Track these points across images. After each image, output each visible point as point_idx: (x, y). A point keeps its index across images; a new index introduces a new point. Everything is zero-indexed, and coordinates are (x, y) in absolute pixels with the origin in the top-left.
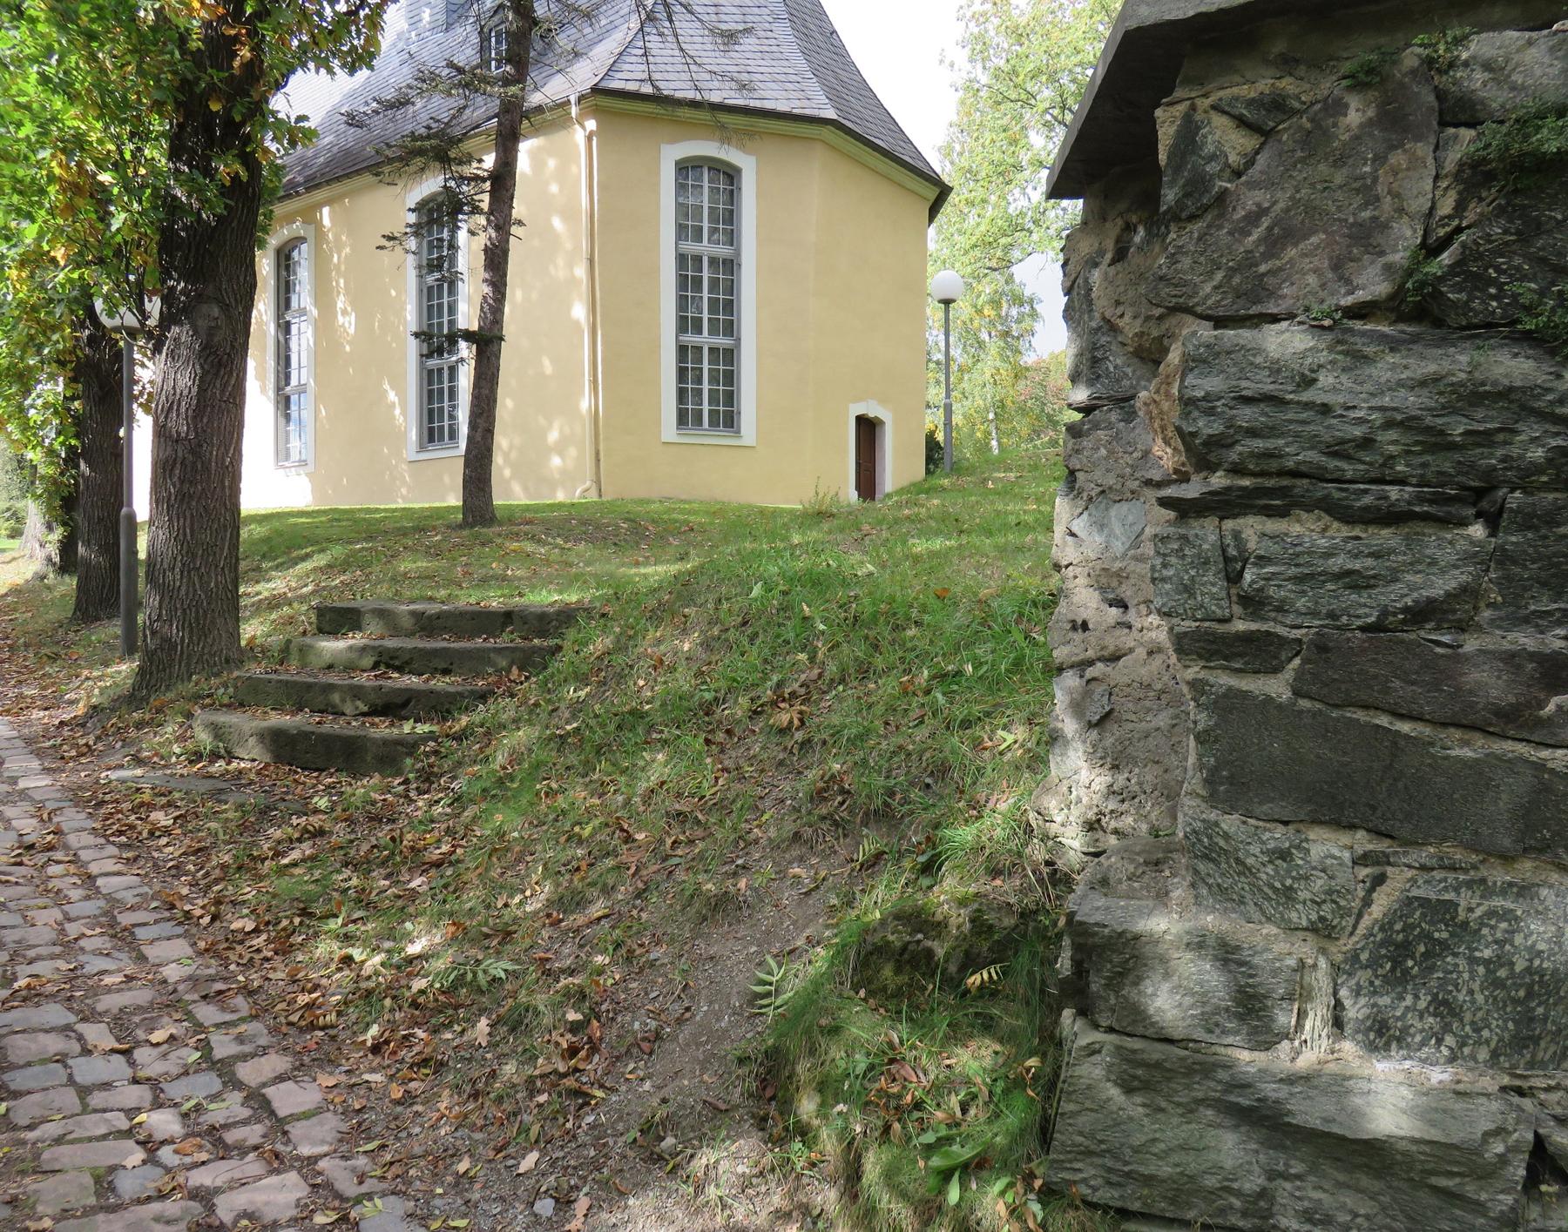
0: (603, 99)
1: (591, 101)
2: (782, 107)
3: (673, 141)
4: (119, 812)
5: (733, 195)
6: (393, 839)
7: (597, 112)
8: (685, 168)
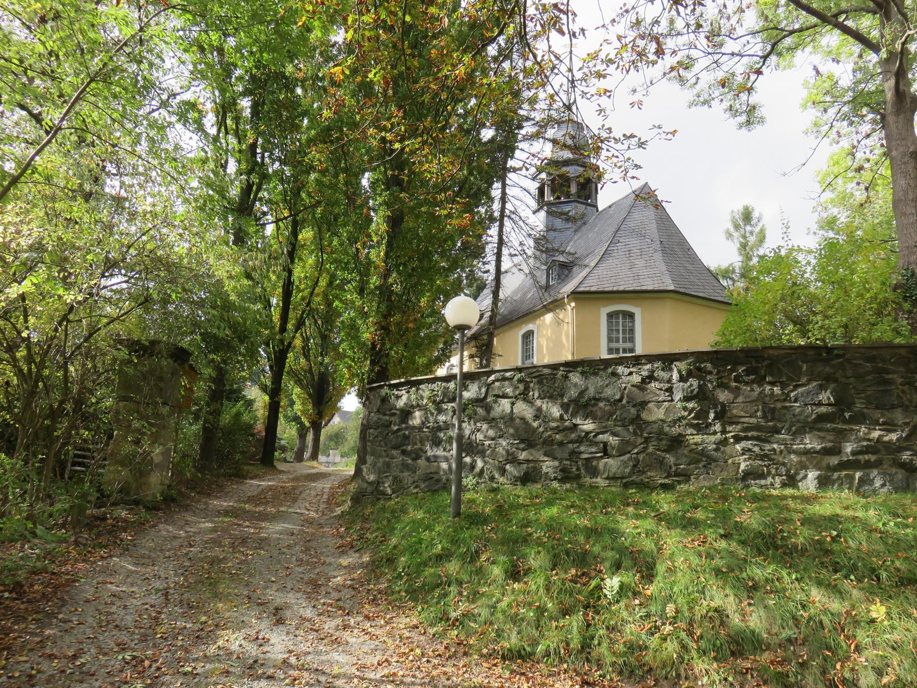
0: (577, 295)
1: (573, 296)
2: (650, 288)
3: (607, 306)
4: (149, 557)
5: (633, 321)
6: (873, 621)
7: (575, 300)
8: (610, 316)
